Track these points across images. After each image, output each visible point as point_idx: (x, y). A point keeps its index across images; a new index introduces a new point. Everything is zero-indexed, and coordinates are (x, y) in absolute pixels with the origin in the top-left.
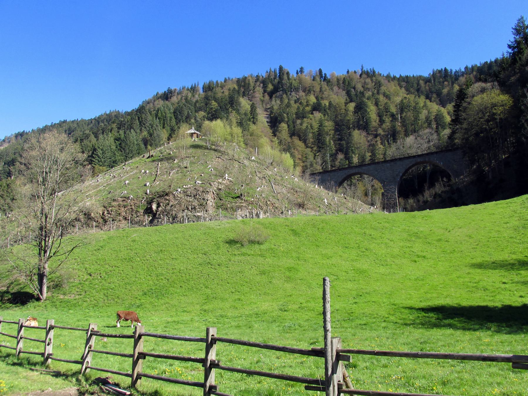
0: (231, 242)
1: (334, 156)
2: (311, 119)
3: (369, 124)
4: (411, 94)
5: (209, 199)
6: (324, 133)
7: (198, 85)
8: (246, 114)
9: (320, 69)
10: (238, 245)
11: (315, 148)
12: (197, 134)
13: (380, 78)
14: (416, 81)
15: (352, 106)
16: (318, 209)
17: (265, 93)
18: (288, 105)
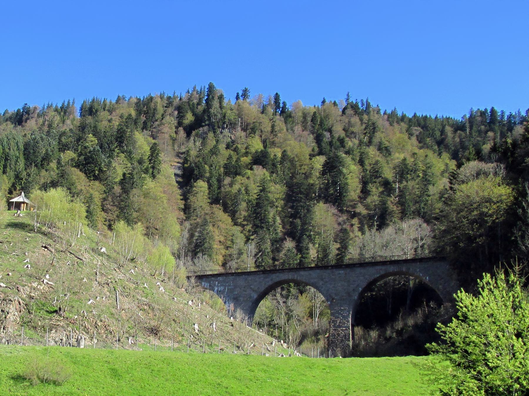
0: (18, 378)
1: (277, 243)
2: (248, 178)
3: (344, 194)
4: (428, 147)
5: (11, 311)
6: (266, 203)
7: (73, 103)
8: (140, 162)
9: (277, 94)
10: (25, 384)
11: (249, 227)
12: (27, 204)
13: (374, 117)
14: (440, 127)
15: (320, 160)
16: (180, 338)
17: (180, 126)
18: (214, 152)
